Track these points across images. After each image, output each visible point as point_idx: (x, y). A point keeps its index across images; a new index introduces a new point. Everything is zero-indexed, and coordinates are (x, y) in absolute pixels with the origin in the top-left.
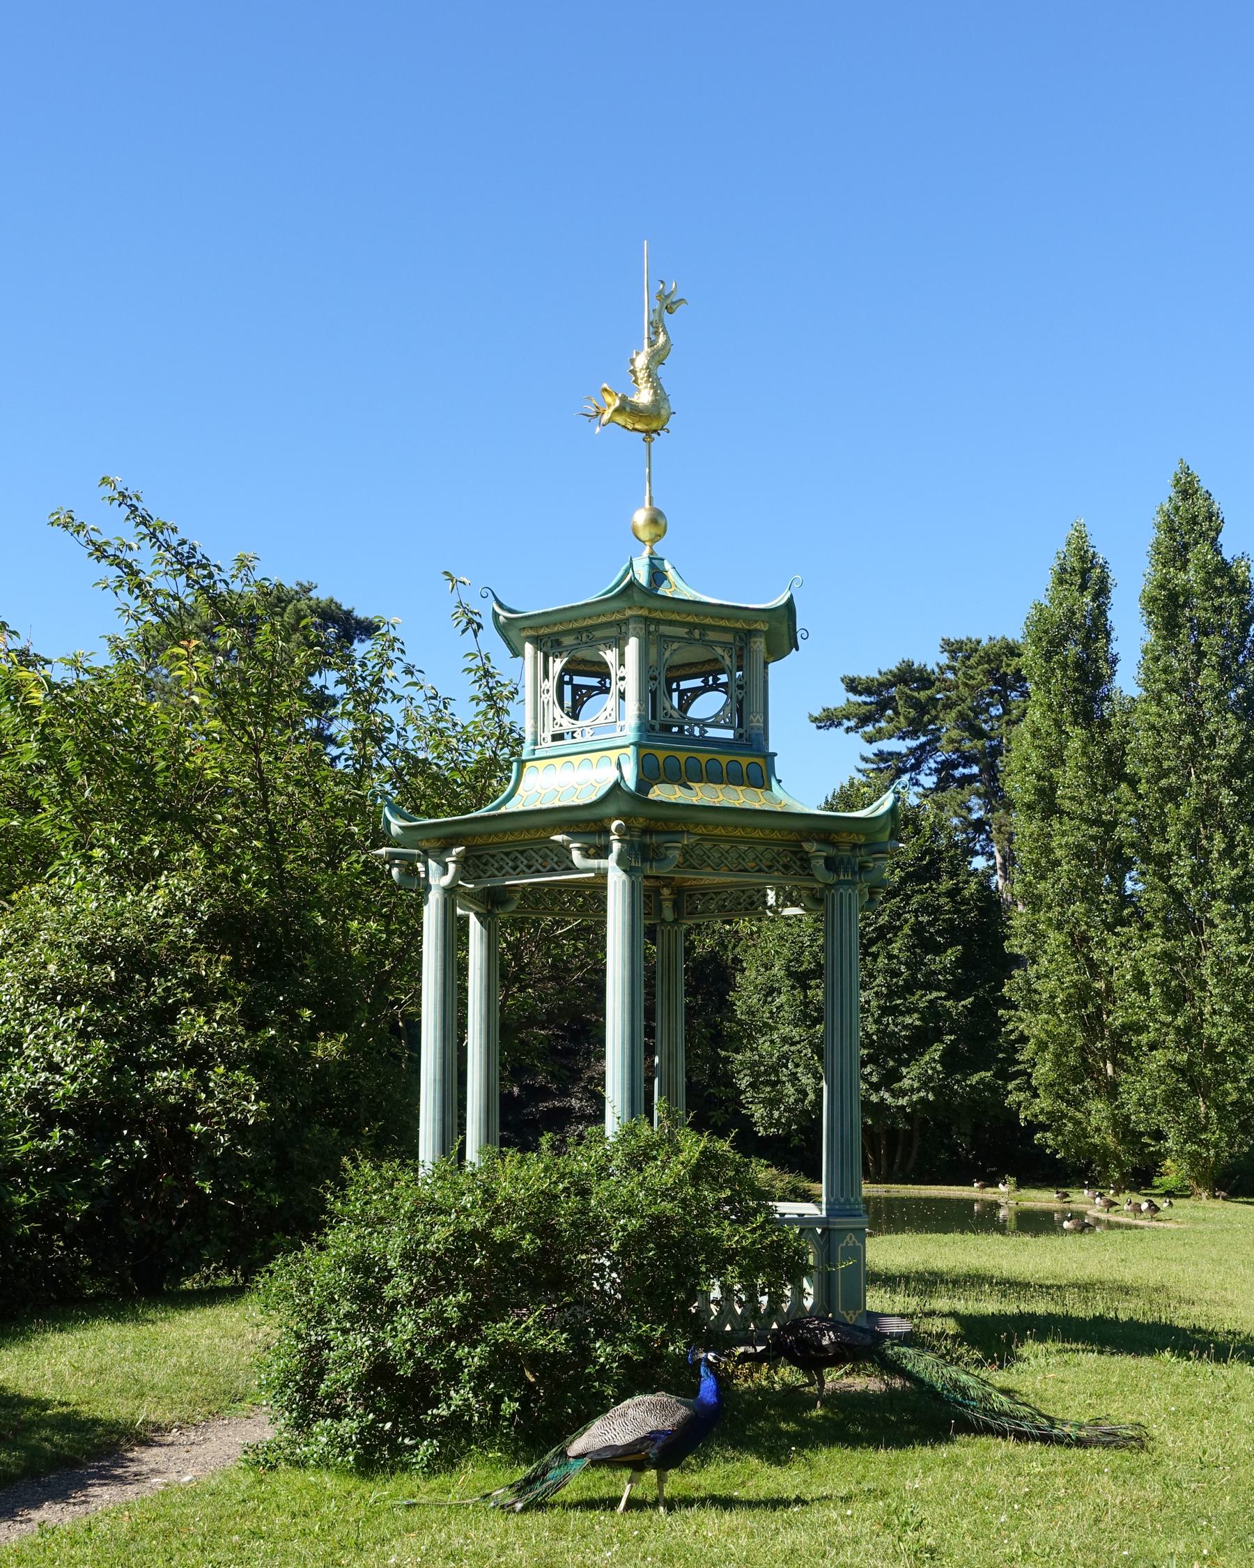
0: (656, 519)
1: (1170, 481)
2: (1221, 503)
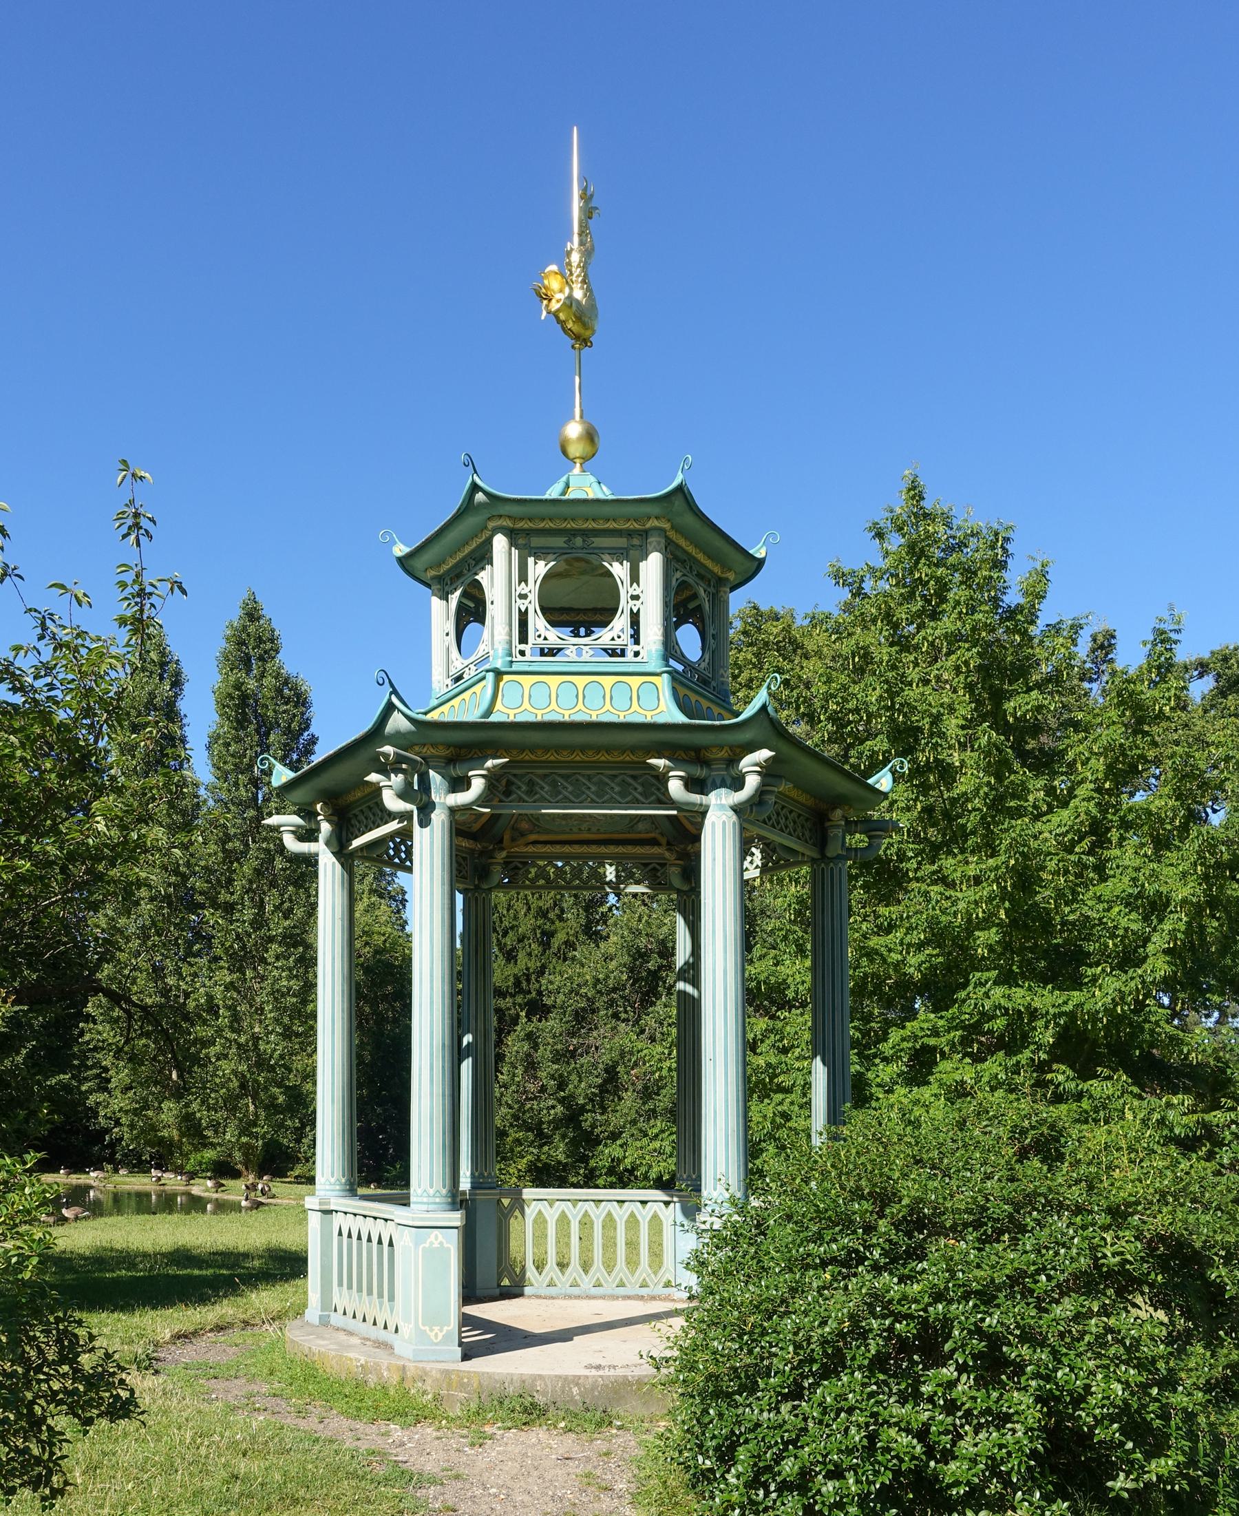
0: (590, 436)
1: (240, 603)
2: (281, 628)
